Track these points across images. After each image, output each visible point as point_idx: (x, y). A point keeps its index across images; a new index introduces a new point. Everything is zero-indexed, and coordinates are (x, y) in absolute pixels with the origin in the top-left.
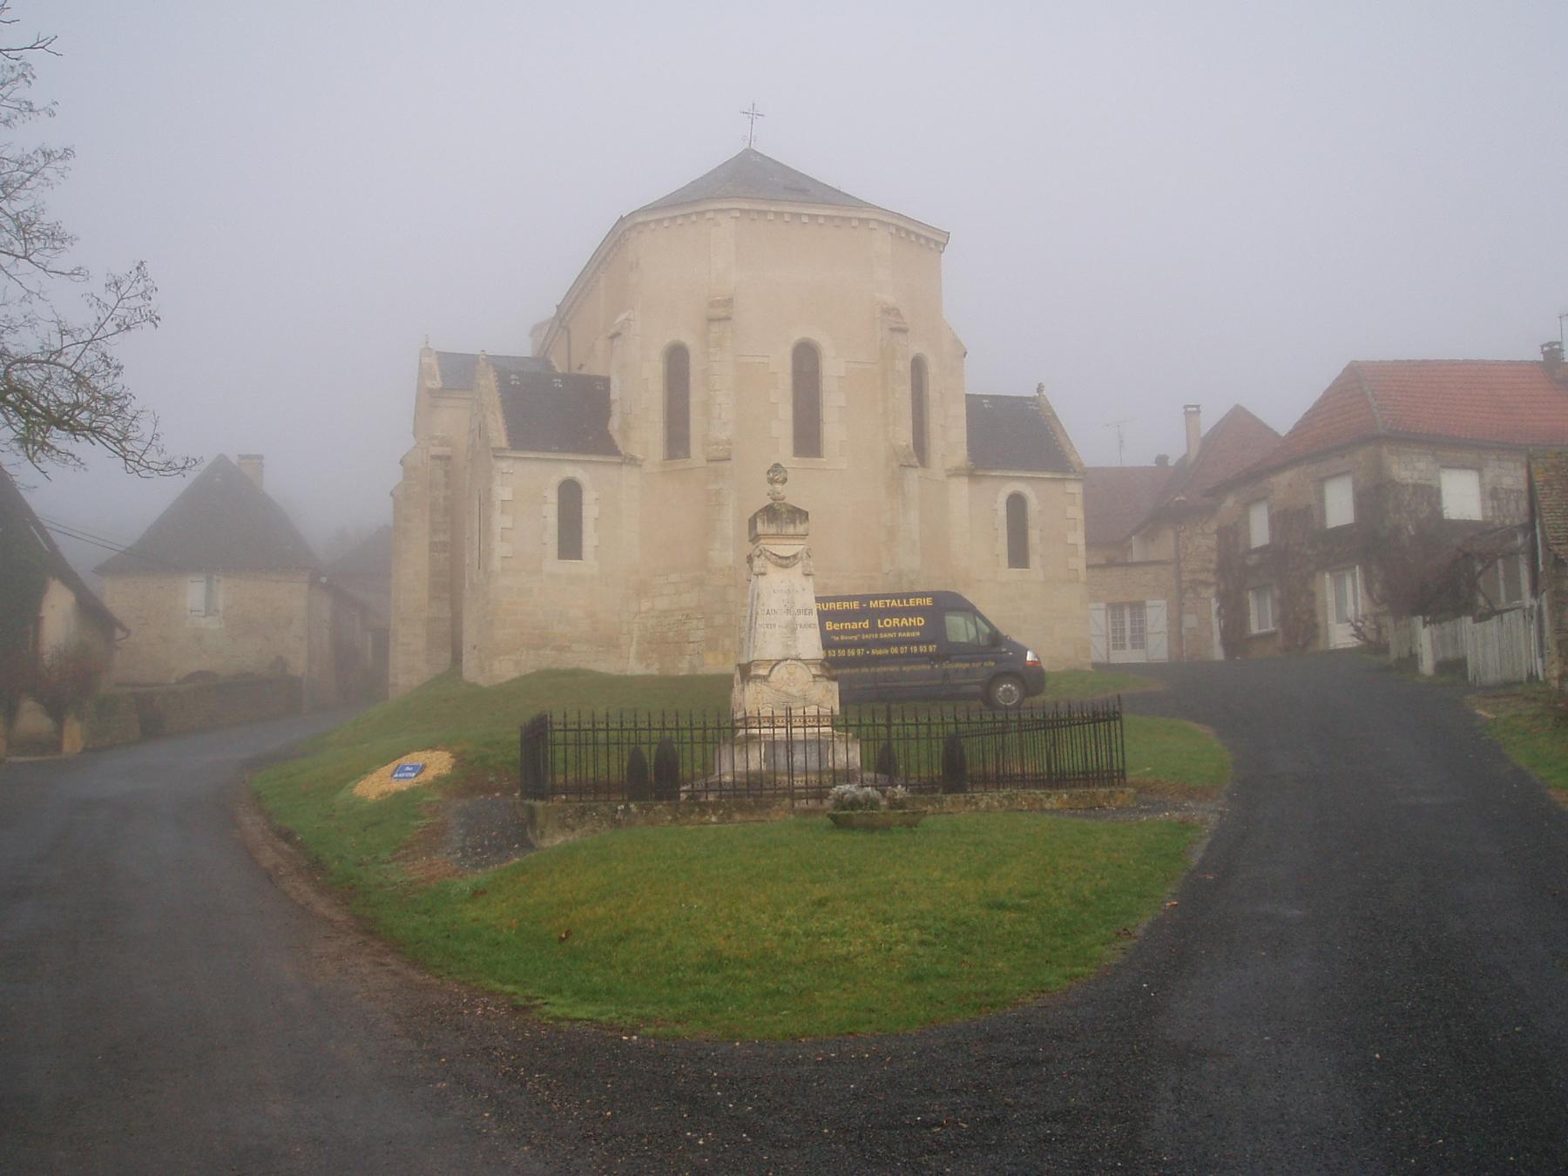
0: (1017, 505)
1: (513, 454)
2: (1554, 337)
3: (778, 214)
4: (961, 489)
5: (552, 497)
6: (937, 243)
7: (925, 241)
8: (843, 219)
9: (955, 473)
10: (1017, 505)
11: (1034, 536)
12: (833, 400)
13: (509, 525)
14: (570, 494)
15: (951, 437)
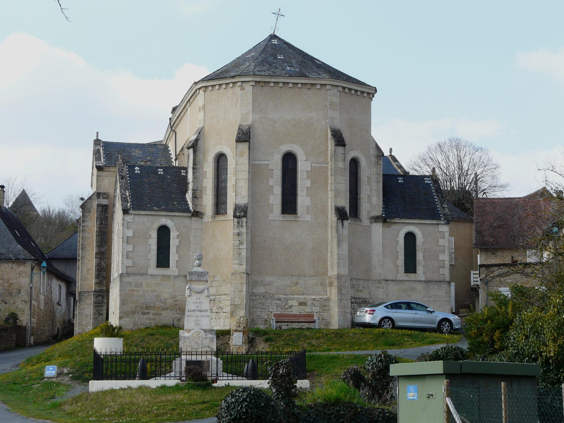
0: (410, 238)
1: (133, 212)
2: (248, 122)
3: (295, 84)
4: (378, 228)
5: (154, 234)
6: (369, 94)
7: (361, 92)
8: (312, 84)
9: (376, 219)
10: (410, 238)
11: (420, 256)
12: (303, 183)
13: (131, 249)
14: (164, 233)
15: (372, 200)
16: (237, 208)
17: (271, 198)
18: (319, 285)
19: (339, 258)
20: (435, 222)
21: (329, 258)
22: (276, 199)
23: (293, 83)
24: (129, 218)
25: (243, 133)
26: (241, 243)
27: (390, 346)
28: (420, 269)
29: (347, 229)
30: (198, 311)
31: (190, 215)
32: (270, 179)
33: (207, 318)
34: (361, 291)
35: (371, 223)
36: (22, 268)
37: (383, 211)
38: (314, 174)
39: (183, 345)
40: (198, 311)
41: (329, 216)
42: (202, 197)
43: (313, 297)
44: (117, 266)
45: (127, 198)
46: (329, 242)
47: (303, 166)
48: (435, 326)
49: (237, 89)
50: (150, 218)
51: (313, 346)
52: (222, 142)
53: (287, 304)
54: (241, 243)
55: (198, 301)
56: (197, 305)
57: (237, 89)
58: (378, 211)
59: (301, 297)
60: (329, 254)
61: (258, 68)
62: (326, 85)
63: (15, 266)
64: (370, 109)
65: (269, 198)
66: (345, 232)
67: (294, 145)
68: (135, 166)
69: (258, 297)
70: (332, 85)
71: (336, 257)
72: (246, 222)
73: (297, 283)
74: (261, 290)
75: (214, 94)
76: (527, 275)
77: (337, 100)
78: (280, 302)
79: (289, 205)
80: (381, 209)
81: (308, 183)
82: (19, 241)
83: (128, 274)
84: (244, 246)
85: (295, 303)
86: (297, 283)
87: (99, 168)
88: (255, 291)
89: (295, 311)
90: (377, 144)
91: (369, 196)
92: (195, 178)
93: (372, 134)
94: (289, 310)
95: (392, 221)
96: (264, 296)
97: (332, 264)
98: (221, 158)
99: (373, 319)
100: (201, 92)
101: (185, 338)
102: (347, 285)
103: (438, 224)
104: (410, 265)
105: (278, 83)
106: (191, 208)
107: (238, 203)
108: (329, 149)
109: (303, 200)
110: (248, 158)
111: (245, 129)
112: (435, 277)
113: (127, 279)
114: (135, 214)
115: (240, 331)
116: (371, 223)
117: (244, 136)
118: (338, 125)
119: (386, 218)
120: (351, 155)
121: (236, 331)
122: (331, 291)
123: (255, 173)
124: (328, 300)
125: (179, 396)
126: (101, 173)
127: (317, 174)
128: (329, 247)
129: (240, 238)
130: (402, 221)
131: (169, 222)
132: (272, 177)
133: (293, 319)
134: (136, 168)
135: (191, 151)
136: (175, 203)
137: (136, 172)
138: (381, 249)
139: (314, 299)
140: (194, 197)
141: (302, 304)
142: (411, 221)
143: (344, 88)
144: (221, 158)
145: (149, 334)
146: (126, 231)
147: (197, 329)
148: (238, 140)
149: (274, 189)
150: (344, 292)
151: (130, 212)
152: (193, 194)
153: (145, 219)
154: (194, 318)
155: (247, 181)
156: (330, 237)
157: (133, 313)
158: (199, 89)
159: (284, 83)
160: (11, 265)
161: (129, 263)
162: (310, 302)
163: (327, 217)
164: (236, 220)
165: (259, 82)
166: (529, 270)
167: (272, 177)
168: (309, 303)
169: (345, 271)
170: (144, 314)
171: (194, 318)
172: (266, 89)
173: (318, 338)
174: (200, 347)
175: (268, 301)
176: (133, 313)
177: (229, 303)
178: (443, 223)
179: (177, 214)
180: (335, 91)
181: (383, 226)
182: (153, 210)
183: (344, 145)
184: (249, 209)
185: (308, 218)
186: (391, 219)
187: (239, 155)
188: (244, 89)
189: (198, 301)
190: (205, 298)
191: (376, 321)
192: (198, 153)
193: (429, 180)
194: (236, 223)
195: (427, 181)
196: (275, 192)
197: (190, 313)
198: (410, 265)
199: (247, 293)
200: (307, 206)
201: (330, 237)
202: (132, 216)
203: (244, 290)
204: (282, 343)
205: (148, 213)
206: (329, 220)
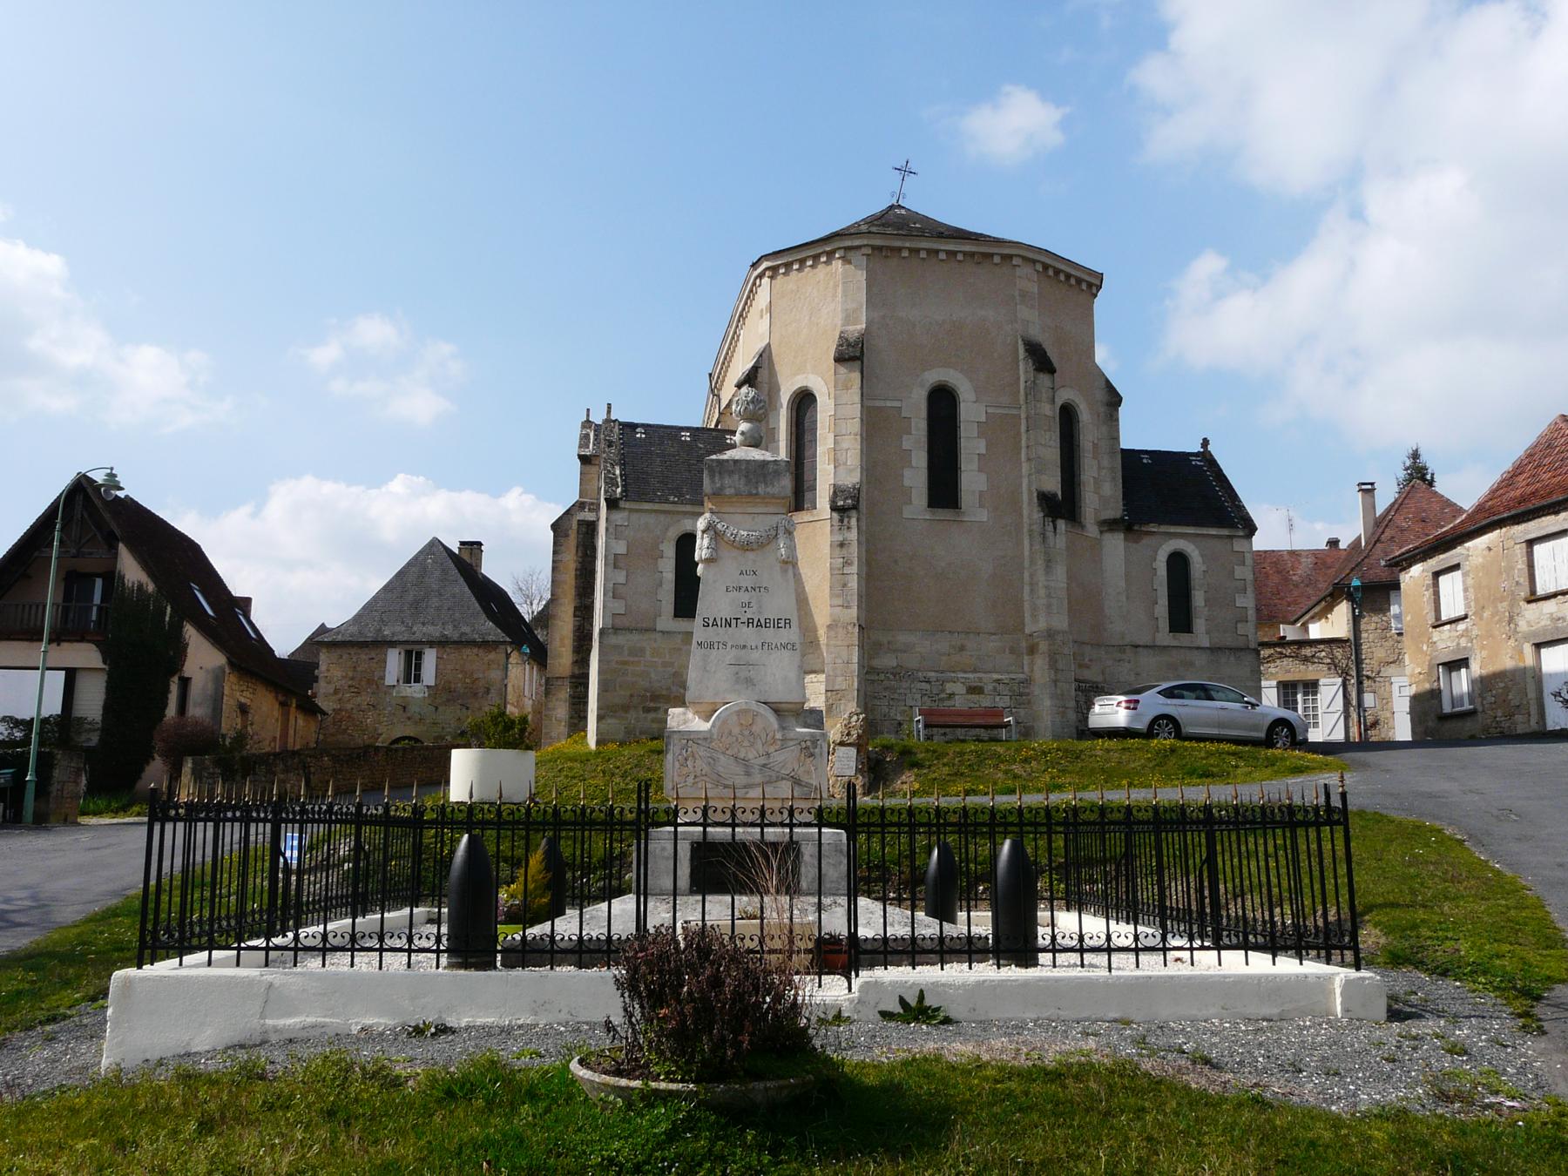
0: (1178, 563)
1: (628, 505)
4: (1115, 544)
6: (1090, 285)
9: (1110, 525)
10: (1178, 563)
11: (1198, 599)
12: (971, 446)
15: (1101, 492)
16: (837, 491)
17: (907, 473)
19: (1049, 596)
20: (1225, 532)
21: (1026, 596)
22: (916, 476)
24: (619, 517)
26: (847, 563)
27: (1201, 776)
28: (1199, 624)
30: (750, 622)
33: (786, 654)
34: (1088, 667)
36: (492, 656)
38: (995, 428)
39: (679, 780)
40: (750, 622)
41: (1025, 513)
43: (996, 676)
44: (598, 623)
46: (1027, 564)
47: (970, 412)
48: (1262, 735)
49: (837, 265)
50: (662, 517)
51: (1016, 777)
52: (810, 369)
53: (943, 691)
54: (847, 563)
55: (747, 581)
56: (745, 597)
57: (837, 265)
58: (1115, 510)
59: (971, 676)
60: (1027, 589)
63: (481, 652)
64: (1092, 315)
67: (952, 371)
69: (882, 677)
71: (1042, 592)
73: (962, 648)
74: (888, 661)
75: (790, 282)
76: (1306, 660)
77: (1034, 288)
78: (927, 686)
79: (944, 489)
81: (981, 447)
82: (490, 615)
83: (616, 630)
84: (854, 569)
85: (959, 689)
86: (962, 648)
87: (584, 460)
88: (876, 663)
89: (961, 702)
90: (1107, 381)
93: (1097, 360)
94: (947, 703)
96: (898, 673)
97: (1034, 608)
98: (804, 401)
99: (1132, 719)
100: (766, 280)
101: (691, 738)
102: (1066, 651)
103: (1231, 537)
104: (1181, 619)
105: (937, 252)
108: (1022, 379)
109: (971, 480)
112: (1229, 641)
113: (613, 640)
114: (631, 510)
115: (850, 745)
117: (851, 354)
118: (1037, 334)
119: (1131, 523)
120: (1064, 396)
121: (842, 744)
122: (1032, 663)
123: (876, 425)
124: (1028, 682)
125: (863, 518)
126: (588, 468)
127: (1000, 429)
128: (1026, 575)
129: (844, 551)
130: (1163, 529)
133: (960, 720)
138: (1123, 584)
139: (998, 681)
141: (975, 690)
145: (652, 751)
146: (613, 542)
147: (739, 700)
148: (839, 359)
150: (1060, 665)
151: (622, 504)
153: (651, 519)
154: (730, 655)
156: (1027, 553)
157: (626, 708)
158: (761, 276)
159: (929, 251)
160: (475, 650)
161: (619, 607)
162: (990, 687)
163: (1021, 515)
164: (835, 515)
166: (1307, 651)
168: (989, 688)
170: (648, 710)
171: (730, 655)
173: (1026, 761)
174: (758, 778)
175: (905, 685)
176: (626, 708)
177: (823, 688)
181: (1126, 539)
182: (667, 501)
184: (863, 495)
185: (983, 516)
187: (840, 386)
189: (747, 581)
190: (778, 567)
191: (1141, 725)
194: (836, 523)
195: (1195, 462)
197: (711, 634)
198: (1181, 619)
199: (861, 665)
201: (1027, 553)
202: (626, 514)
203: (855, 660)
204: (946, 770)
205: (657, 507)
206: (1026, 519)
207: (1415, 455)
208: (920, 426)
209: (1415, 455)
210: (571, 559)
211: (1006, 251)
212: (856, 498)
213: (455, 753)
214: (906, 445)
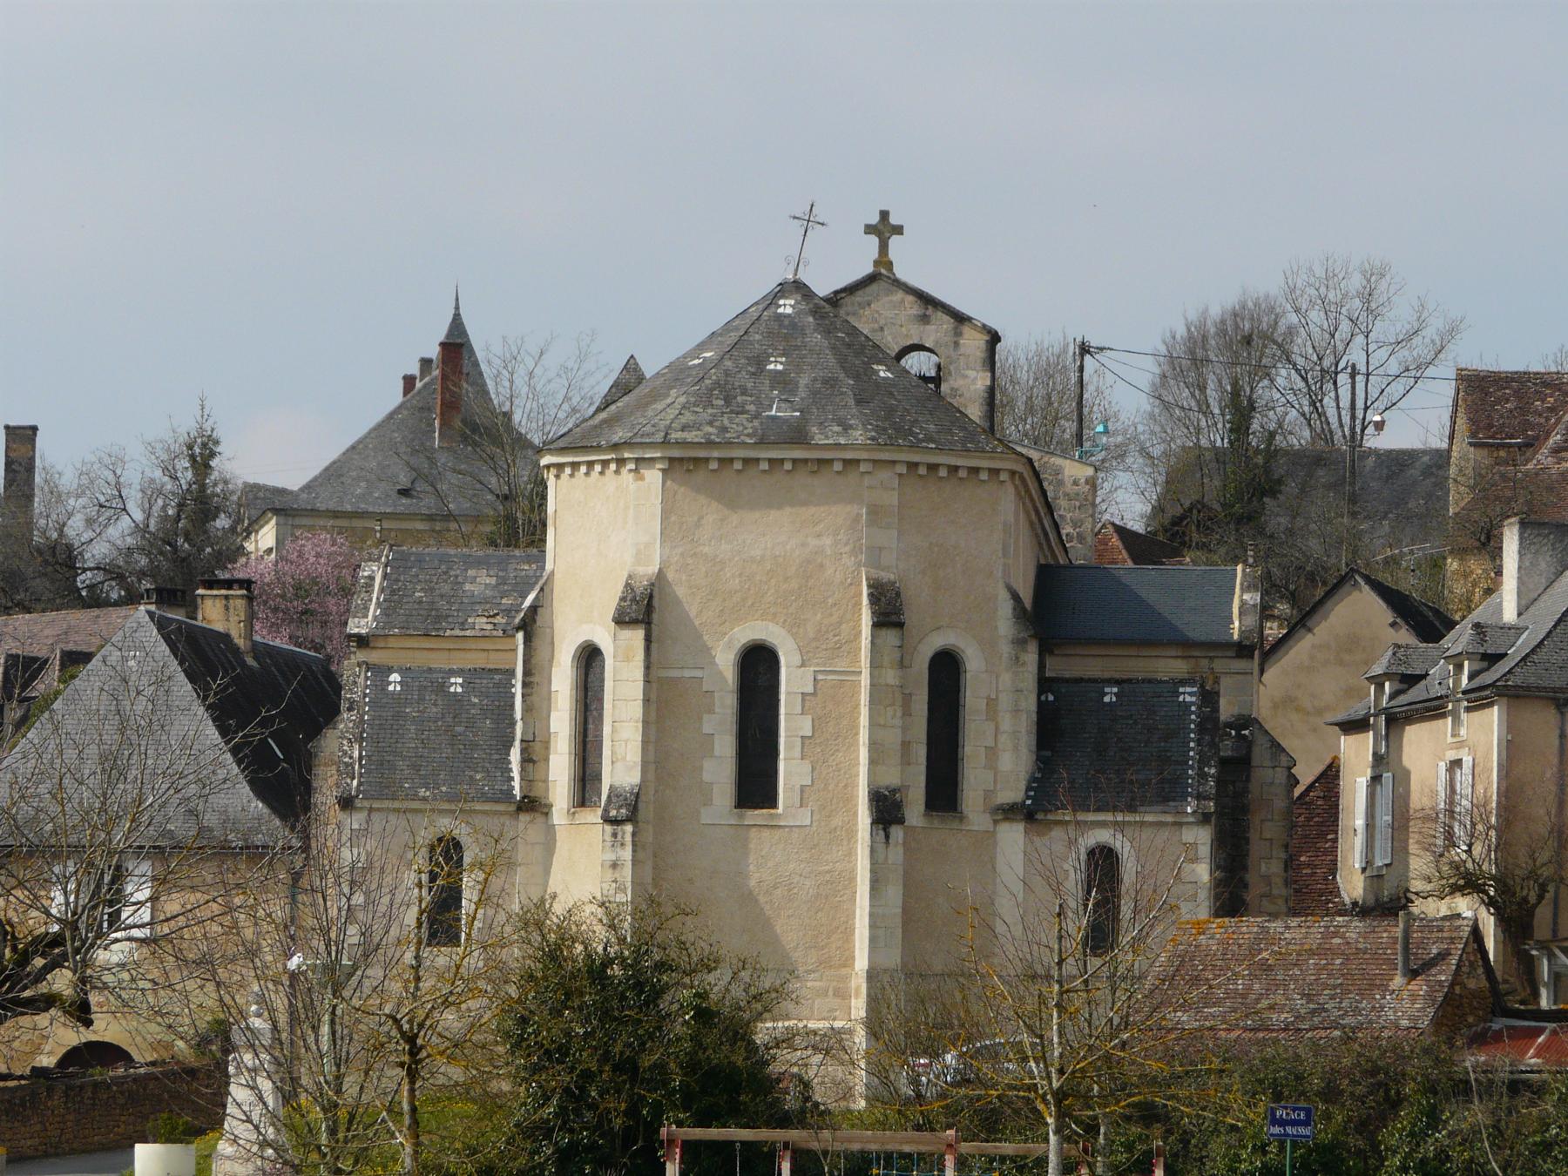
0: (1103, 863)
4: (1013, 836)
9: (1009, 812)
10: (1103, 863)
12: (791, 725)
17: (708, 765)
18: (831, 993)
22: (719, 767)
23: (770, 461)
25: (634, 600)
29: (900, 850)
31: (513, 808)
32: (706, 717)
35: (996, 822)
37: (1028, 789)
42: (547, 760)
45: (352, 765)
47: (792, 681)
57: (626, 475)
58: (1014, 791)
61: (688, 417)
62: (858, 461)
65: (701, 768)
66: (896, 854)
68: (390, 670)
70: (874, 461)
72: (634, 834)
77: (892, 499)
80: (1022, 786)
91: (992, 752)
92: (527, 709)
95: (1050, 817)
98: (590, 657)
104: (1100, 937)
105: (731, 460)
106: (517, 792)
107: (617, 784)
109: (790, 770)
110: (641, 664)
111: (641, 585)
116: (996, 822)
119: (1031, 811)
123: (664, 700)
131: (462, 832)
132: (711, 711)
134: (395, 677)
135: (520, 636)
136: (478, 777)
137: (391, 688)
140: (527, 760)
142: (1101, 817)
143: (912, 466)
144: (590, 657)
149: (717, 746)
151: (358, 803)
152: (523, 751)
155: (640, 725)
164: (609, 828)
165: (681, 460)
167: (711, 711)
169: (893, 958)
172: (700, 476)
178: (1191, 819)
179: (478, 807)
180: (885, 475)
183: (900, 625)
186: (1047, 811)
188: (642, 478)
192: (536, 642)
193: (1190, 694)
194: (608, 838)
196: (717, 753)
200: (803, 788)
207: (456, 349)
208: (726, 704)
209: (456, 349)
210: (590, 760)
211: (849, 455)
212: (634, 809)
213: (138, 1146)
214: (707, 729)
